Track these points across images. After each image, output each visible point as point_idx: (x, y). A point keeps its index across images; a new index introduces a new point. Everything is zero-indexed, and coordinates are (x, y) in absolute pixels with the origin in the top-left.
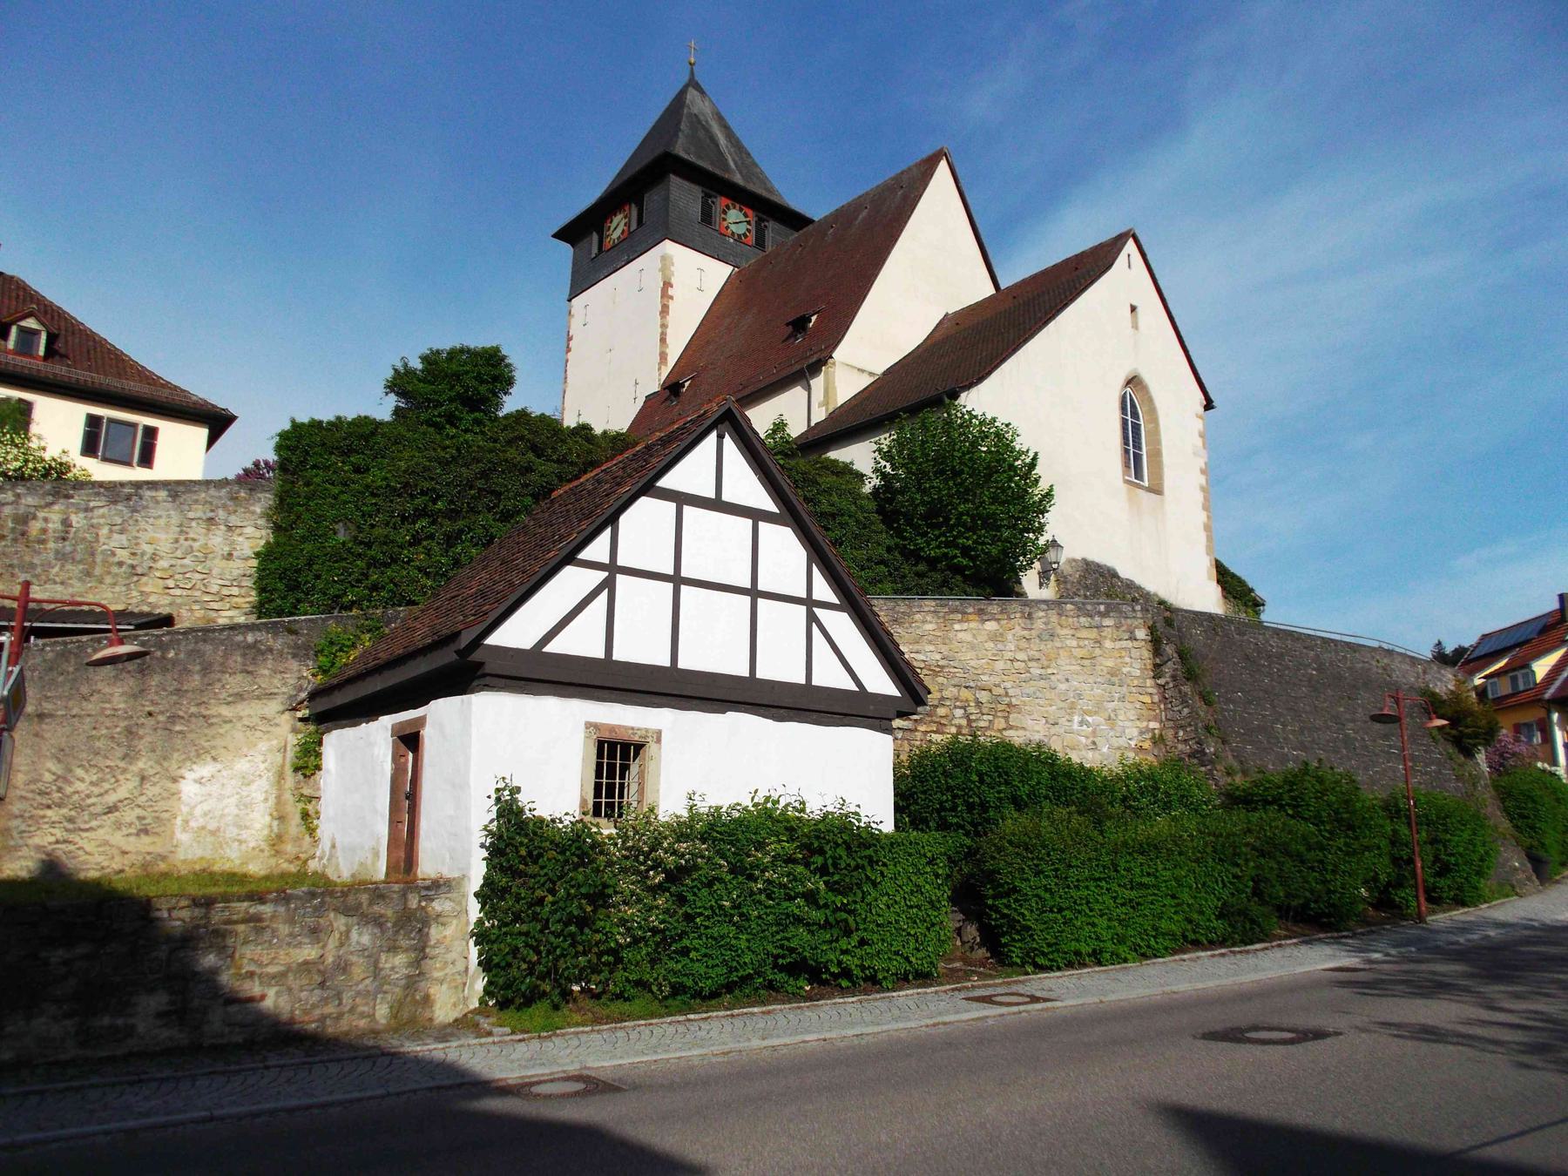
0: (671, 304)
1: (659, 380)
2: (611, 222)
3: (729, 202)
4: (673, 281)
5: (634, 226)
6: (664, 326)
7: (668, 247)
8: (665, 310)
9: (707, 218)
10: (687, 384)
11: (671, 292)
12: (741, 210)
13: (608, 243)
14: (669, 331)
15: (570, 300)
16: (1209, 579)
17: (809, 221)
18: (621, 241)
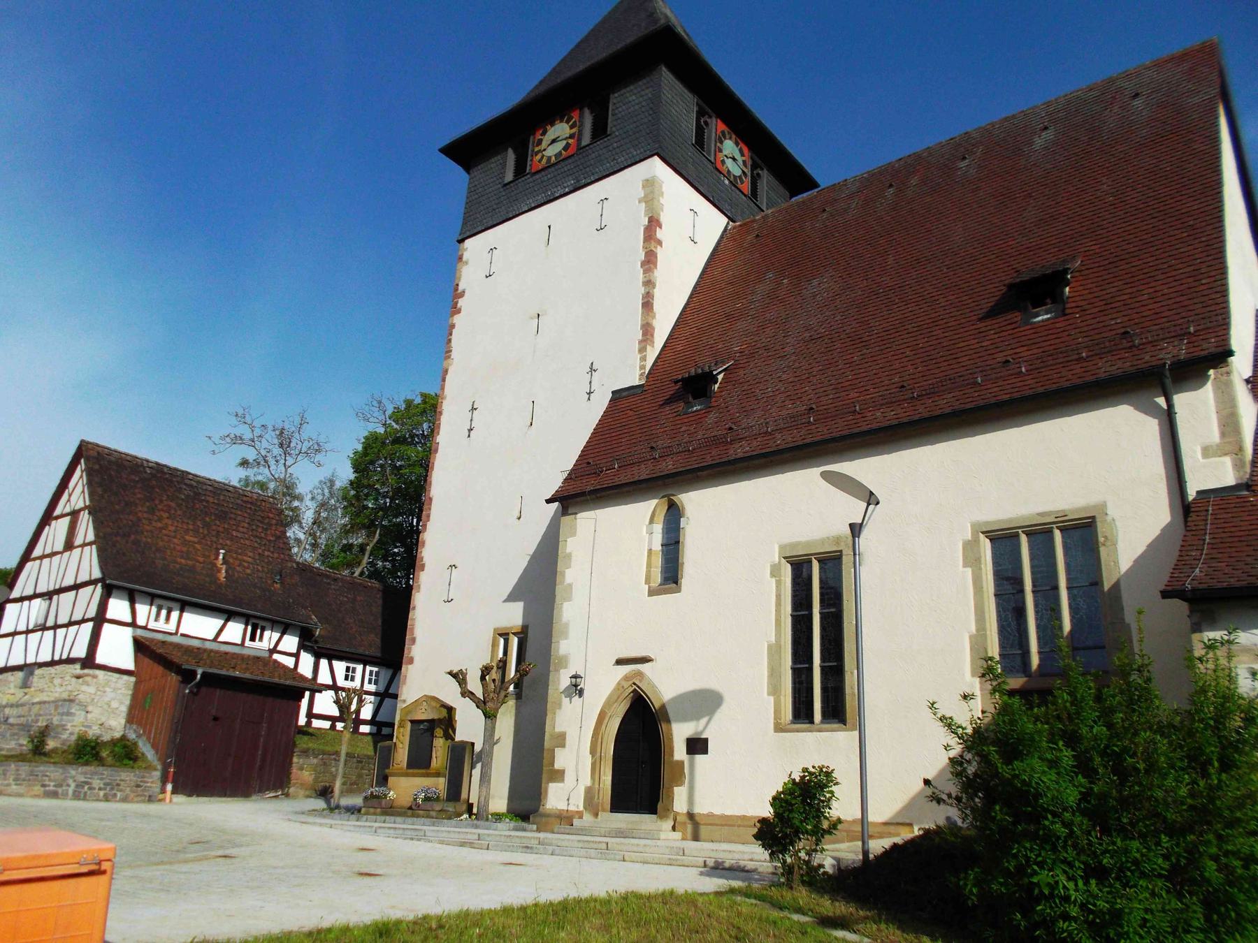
0: (660, 252)
1: (642, 367)
2: (544, 134)
3: (726, 129)
4: (663, 218)
5: (586, 140)
6: (649, 283)
7: (656, 167)
8: (650, 261)
9: (700, 142)
10: (720, 377)
11: (660, 234)
12: (737, 144)
13: (536, 162)
14: (657, 292)
15: (461, 241)
16: (569, 556)
17: (810, 184)
18: (561, 160)
